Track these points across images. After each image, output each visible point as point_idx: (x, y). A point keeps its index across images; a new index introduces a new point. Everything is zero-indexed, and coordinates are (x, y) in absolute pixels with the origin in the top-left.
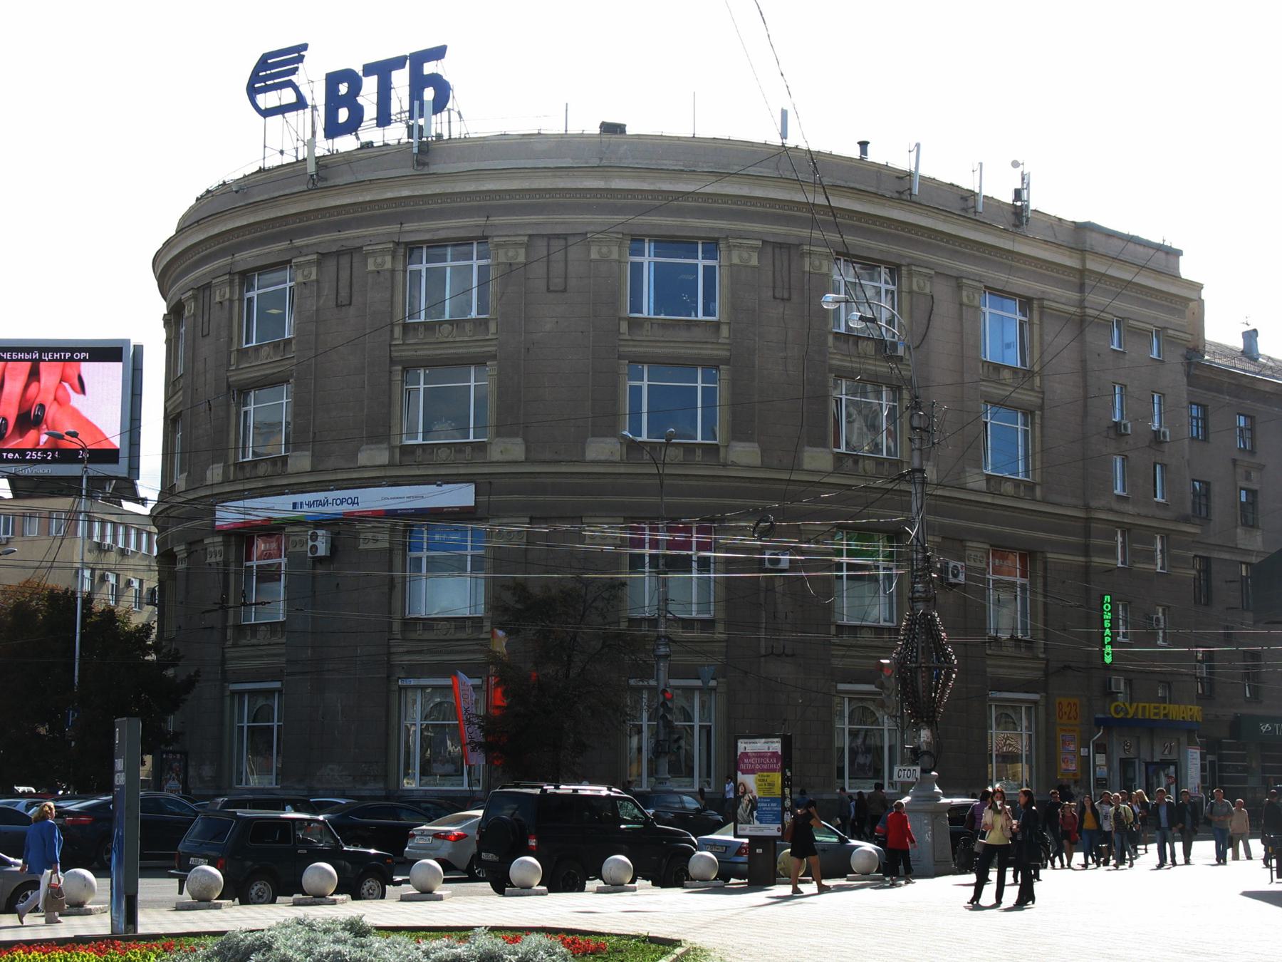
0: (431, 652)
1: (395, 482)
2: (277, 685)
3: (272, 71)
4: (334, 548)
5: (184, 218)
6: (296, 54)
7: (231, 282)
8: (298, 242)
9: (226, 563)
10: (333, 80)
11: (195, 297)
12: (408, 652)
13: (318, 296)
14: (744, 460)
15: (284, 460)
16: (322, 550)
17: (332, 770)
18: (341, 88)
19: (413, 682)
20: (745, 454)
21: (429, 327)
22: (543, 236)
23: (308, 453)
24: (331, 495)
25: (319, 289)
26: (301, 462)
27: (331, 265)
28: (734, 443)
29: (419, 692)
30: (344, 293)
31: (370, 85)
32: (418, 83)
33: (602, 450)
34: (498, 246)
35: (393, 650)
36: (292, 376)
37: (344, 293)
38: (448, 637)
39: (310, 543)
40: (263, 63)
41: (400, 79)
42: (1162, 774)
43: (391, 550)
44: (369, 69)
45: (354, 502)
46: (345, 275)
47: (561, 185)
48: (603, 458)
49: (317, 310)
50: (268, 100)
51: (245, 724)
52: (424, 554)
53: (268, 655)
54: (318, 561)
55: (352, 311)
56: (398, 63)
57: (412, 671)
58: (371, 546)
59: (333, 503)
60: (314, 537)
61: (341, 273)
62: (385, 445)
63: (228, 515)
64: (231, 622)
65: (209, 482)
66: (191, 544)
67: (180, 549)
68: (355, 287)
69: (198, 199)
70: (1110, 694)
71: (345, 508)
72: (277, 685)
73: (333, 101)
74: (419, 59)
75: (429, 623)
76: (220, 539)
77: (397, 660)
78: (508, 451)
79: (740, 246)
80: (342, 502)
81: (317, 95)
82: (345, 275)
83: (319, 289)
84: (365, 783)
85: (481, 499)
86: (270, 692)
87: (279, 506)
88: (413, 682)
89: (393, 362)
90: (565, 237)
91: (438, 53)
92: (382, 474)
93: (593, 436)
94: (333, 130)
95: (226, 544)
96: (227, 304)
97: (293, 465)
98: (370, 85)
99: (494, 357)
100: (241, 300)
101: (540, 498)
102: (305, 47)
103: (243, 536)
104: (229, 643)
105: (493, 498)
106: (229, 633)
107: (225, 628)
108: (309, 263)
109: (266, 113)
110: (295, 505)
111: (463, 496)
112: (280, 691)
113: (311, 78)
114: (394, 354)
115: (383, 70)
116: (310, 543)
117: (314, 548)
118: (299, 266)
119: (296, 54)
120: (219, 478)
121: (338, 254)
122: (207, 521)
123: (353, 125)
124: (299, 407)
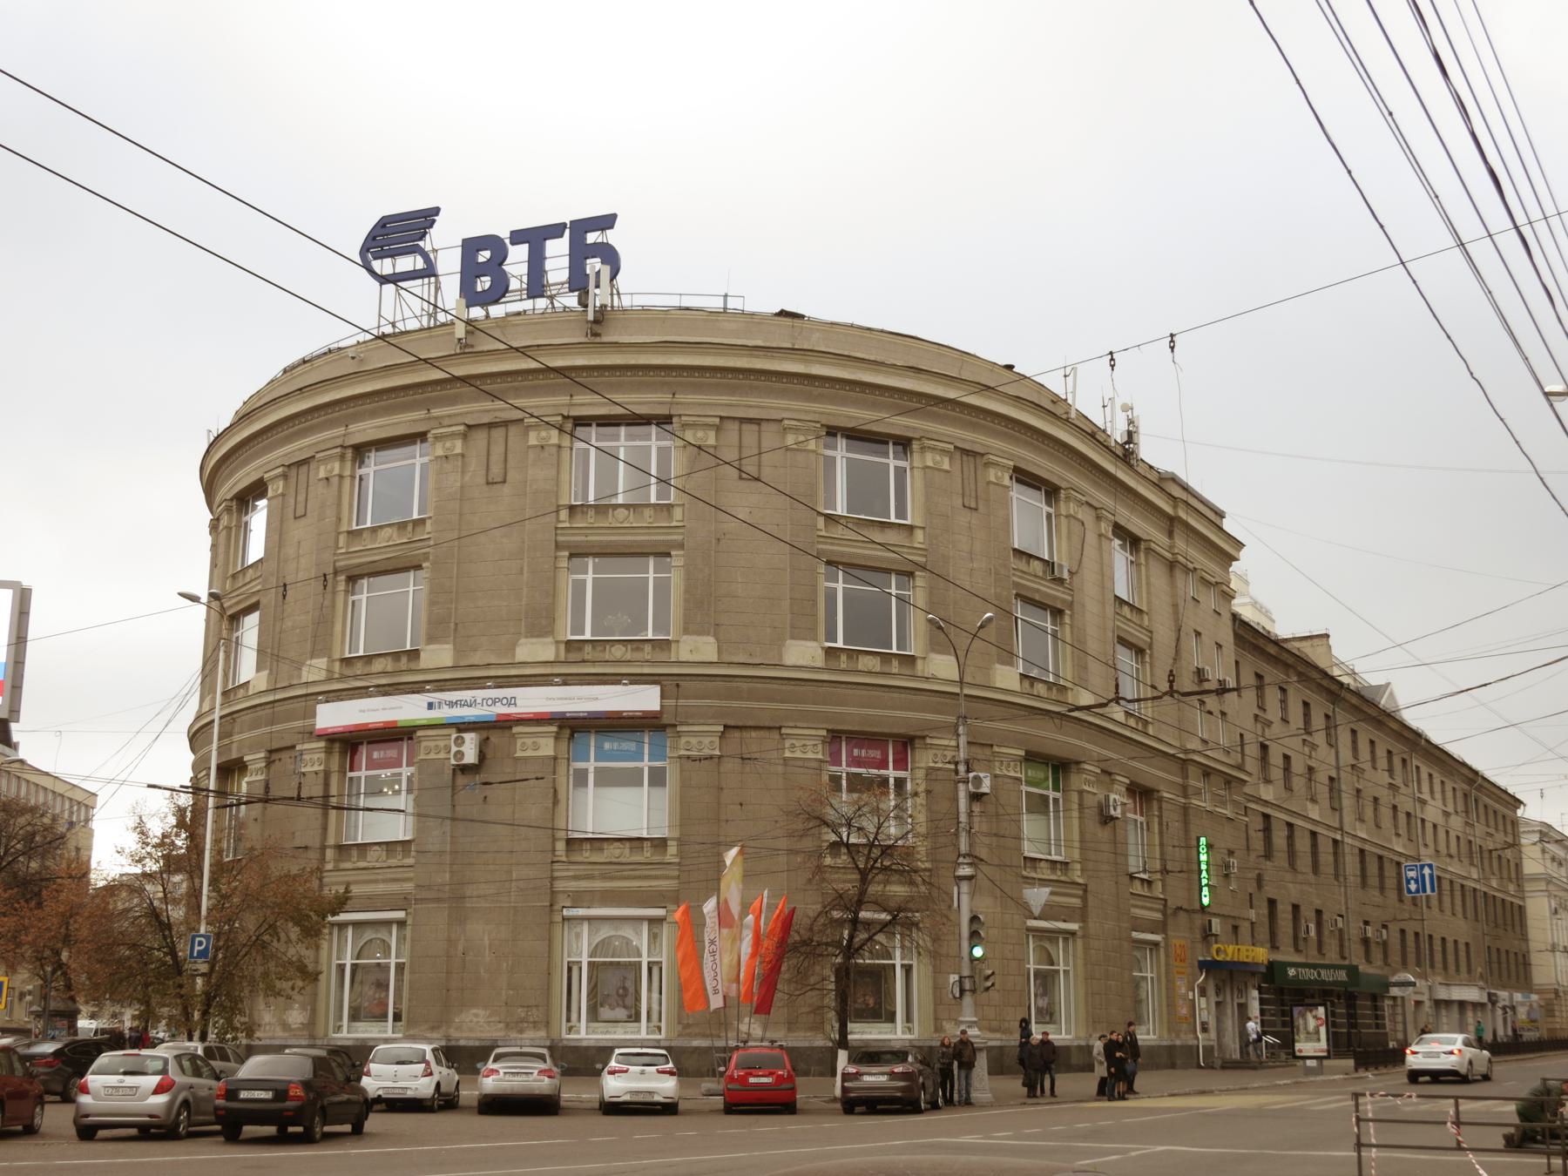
0: (604, 877)
1: (567, 680)
2: (400, 915)
3: (397, 236)
4: (482, 756)
5: (302, 376)
6: (427, 217)
7: (342, 457)
8: (436, 412)
9: (327, 774)
10: (471, 246)
11: (285, 476)
12: (576, 878)
13: (463, 472)
14: (942, 674)
15: (414, 654)
16: (470, 757)
17: (476, 1015)
18: (483, 256)
19: (581, 912)
20: (943, 667)
21: (601, 509)
22: (734, 418)
23: (450, 647)
24: (480, 694)
25: (464, 465)
26: (438, 656)
27: (480, 437)
28: (933, 656)
29: (586, 926)
30: (496, 470)
31: (518, 256)
32: (580, 252)
33: (803, 654)
34: (685, 426)
35: (556, 874)
36: (427, 559)
37: (496, 470)
38: (622, 860)
39: (454, 749)
40: (384, 223)
41: (557, 252)
42: (1309, 1016)
43: (555, 758)
44: (518, 237)
45: (511, 702)
46: (498, 450)
47: (759, 366)
48: (804, 663)
49: (462, 487)
50: (384, 266)
51: (348, 962)
52: (591, 765)
53: (384, 881)
54: (465, 769)
55: (506, 489)
56: (555, 231)
57: (578, 899)
58: (529, 753)
59: (482, 704)
60: (460, 741)
61: (493, 448)
62: (550, 639)
63: (334, 716)
64: (331, 841)
65: (304, 680)
66: (271, 752)
67: (255, 759)
68: (511, 463)
69: (285, 371)
70: (1207, 935)
71: (501, 709)
72: (400, 915)
73: (470, 271)
74: (580, 228)
75: (598, 842)
76: (322, 744)
77: (560, 885)
78: (698, 650)
79: (933, 449)
80: (494, 702)
81: (449, 263)
82: (498, 450)
83: (464, 465)
84: (521, 1031)
85: (667, 702)
86: (387, 923)
87: (407, 709)
88: (581, 912)
89: (558, 546)
90: (758, 421)
91: (607, 222)
92: (548, 670)
93: (792, 638)
94: (470, 296)
95: (328, 751)
96: (335, 481)
97: (426, 660)
98: (518, 256)
99: (681, 546)
100: (353, 477)
101: (735, 704)
102: (436, 211)
103: (349, 743)
104: (329, 866)
105: (682, 702)
106: (330, 853)
107: (323, 848)
108: (453, 435)
109: (394, 279)
110: (430, 706)
111: (646, 699)
112: (401, 924)
113: (445, 242)
114: (560, 538)
115: (536, 238)
116: (454, 749)
117: (460, 755)
118: (437, 438)
119: (427, 217)
120: (322, 675)
121: (491, 426)
122: (308, 722)
123: (499, 292)
124: (437, 594)
